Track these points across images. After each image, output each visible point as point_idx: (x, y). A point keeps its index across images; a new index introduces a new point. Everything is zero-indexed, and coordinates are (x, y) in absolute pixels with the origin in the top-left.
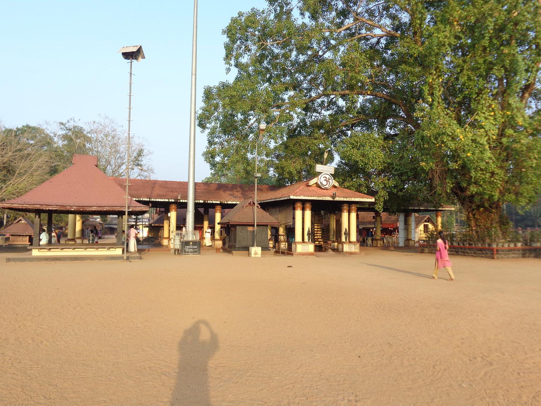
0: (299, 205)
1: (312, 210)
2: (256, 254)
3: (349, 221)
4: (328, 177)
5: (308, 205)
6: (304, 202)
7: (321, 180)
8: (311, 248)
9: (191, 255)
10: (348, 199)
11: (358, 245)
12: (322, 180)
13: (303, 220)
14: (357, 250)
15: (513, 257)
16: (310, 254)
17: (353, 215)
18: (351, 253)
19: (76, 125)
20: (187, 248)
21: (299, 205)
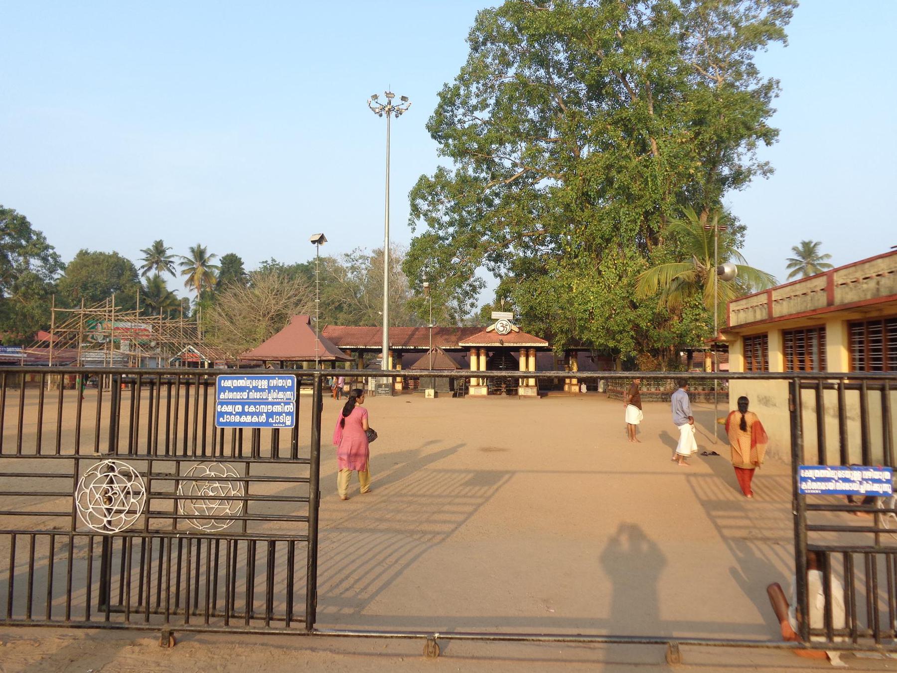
0: (523, 352)
1: (487, 355)
2: (429, 395)
3: (527, 365)
4: (505, 323)
5: (532, 352)
6: (478, 349)
7: (498, 326)
8: (484, 391)
9: (383, 396)
10: (524, 345)
11: (535, 390)
12: (499, 325)
13: (478, 364)
14: (535, 394)
15: (649, 401)
16: (483, 397)
17: (532, 360)
18: (525, 397)
19: (426, 106)
20: (380, 390)
21: (523, 352)
